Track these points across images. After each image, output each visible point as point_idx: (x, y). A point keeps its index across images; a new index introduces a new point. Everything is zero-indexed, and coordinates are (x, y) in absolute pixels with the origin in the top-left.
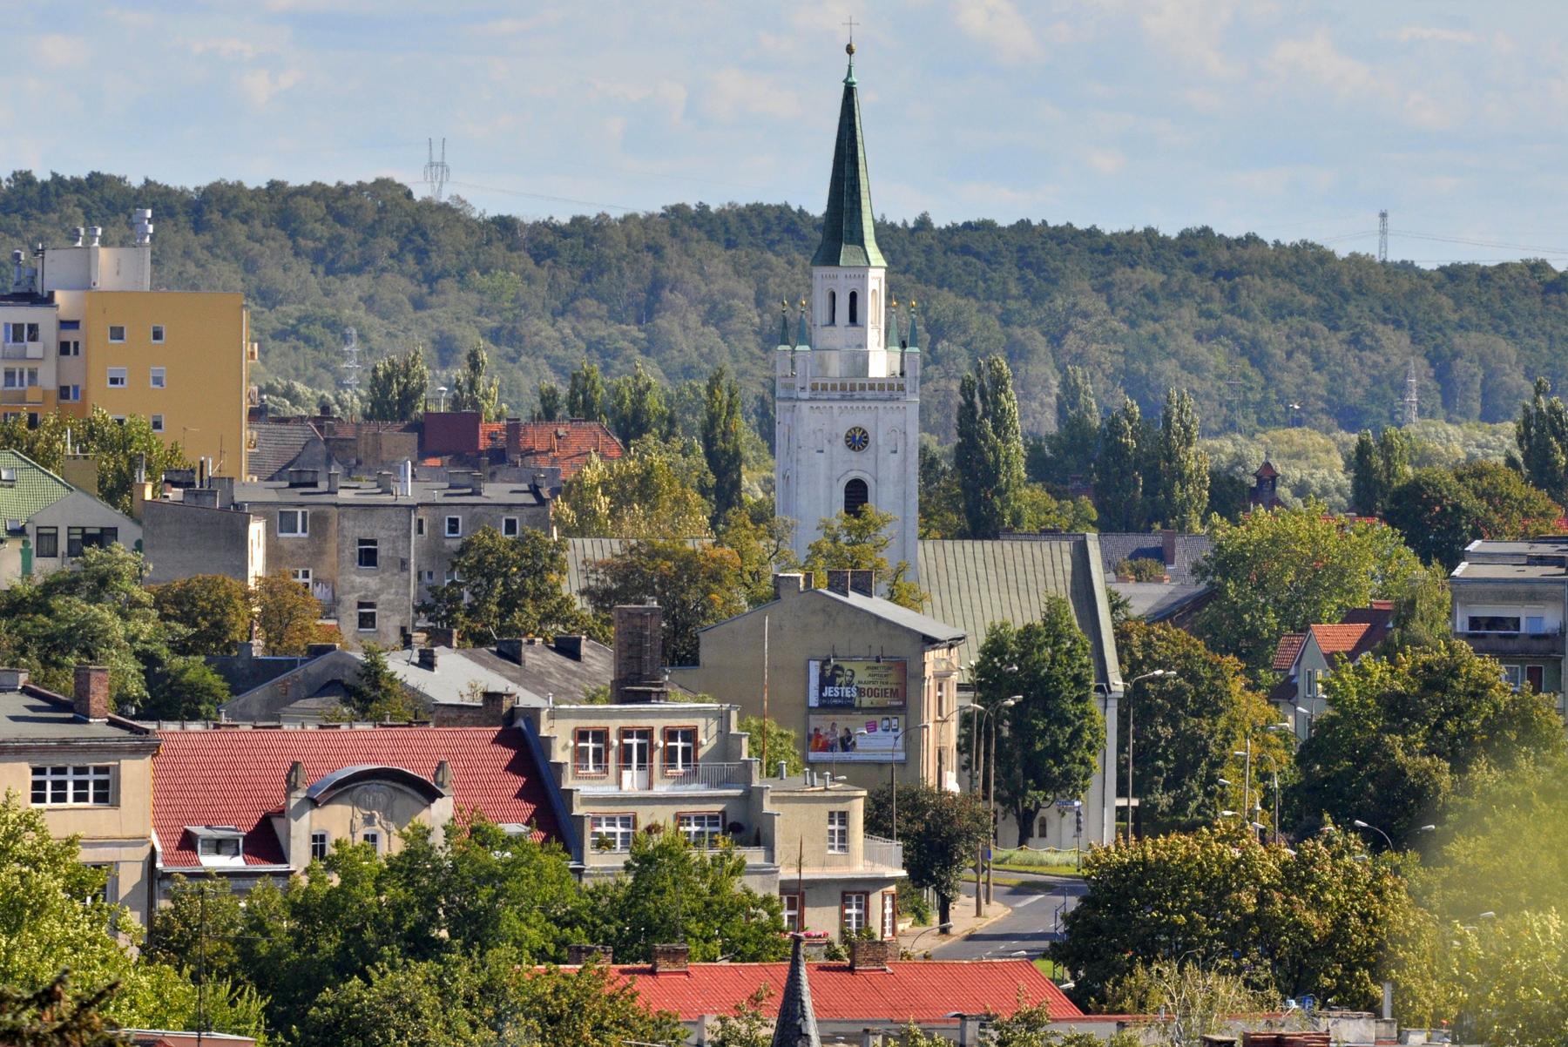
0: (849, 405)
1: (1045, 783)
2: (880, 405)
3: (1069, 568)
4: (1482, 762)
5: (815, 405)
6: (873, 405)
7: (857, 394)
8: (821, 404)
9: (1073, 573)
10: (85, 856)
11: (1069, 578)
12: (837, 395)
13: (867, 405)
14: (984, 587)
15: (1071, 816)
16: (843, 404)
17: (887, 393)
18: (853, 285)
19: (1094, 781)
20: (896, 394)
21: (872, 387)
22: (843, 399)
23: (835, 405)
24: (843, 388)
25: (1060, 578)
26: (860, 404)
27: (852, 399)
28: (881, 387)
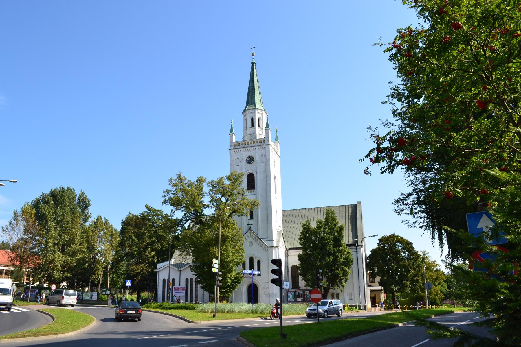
0: (246, 149)
1: (421, 11)
2: (257, 148)
3: (350, 212)
4: (493, 251)
5: (235, 150)
6: (254, 148)
7: (249, 145)
8: (237, 150)
9: (352, 213)
10: (114, 306)
11: (350, 214)
12: (242, 146)
13: (252, 148)
14: (344, 218)
15: (387, 99)
16: (244, 149)
17: (259, 144)
18: (251, 115)
19: (352, 271)
20: (262, 144)
21: (257, 142)
22: (245, 147)
23: (242, 150)
24: (245, 144)
25: (347, 214)
26: (250, 148)
27: (248, 147)
28: (261, 142)
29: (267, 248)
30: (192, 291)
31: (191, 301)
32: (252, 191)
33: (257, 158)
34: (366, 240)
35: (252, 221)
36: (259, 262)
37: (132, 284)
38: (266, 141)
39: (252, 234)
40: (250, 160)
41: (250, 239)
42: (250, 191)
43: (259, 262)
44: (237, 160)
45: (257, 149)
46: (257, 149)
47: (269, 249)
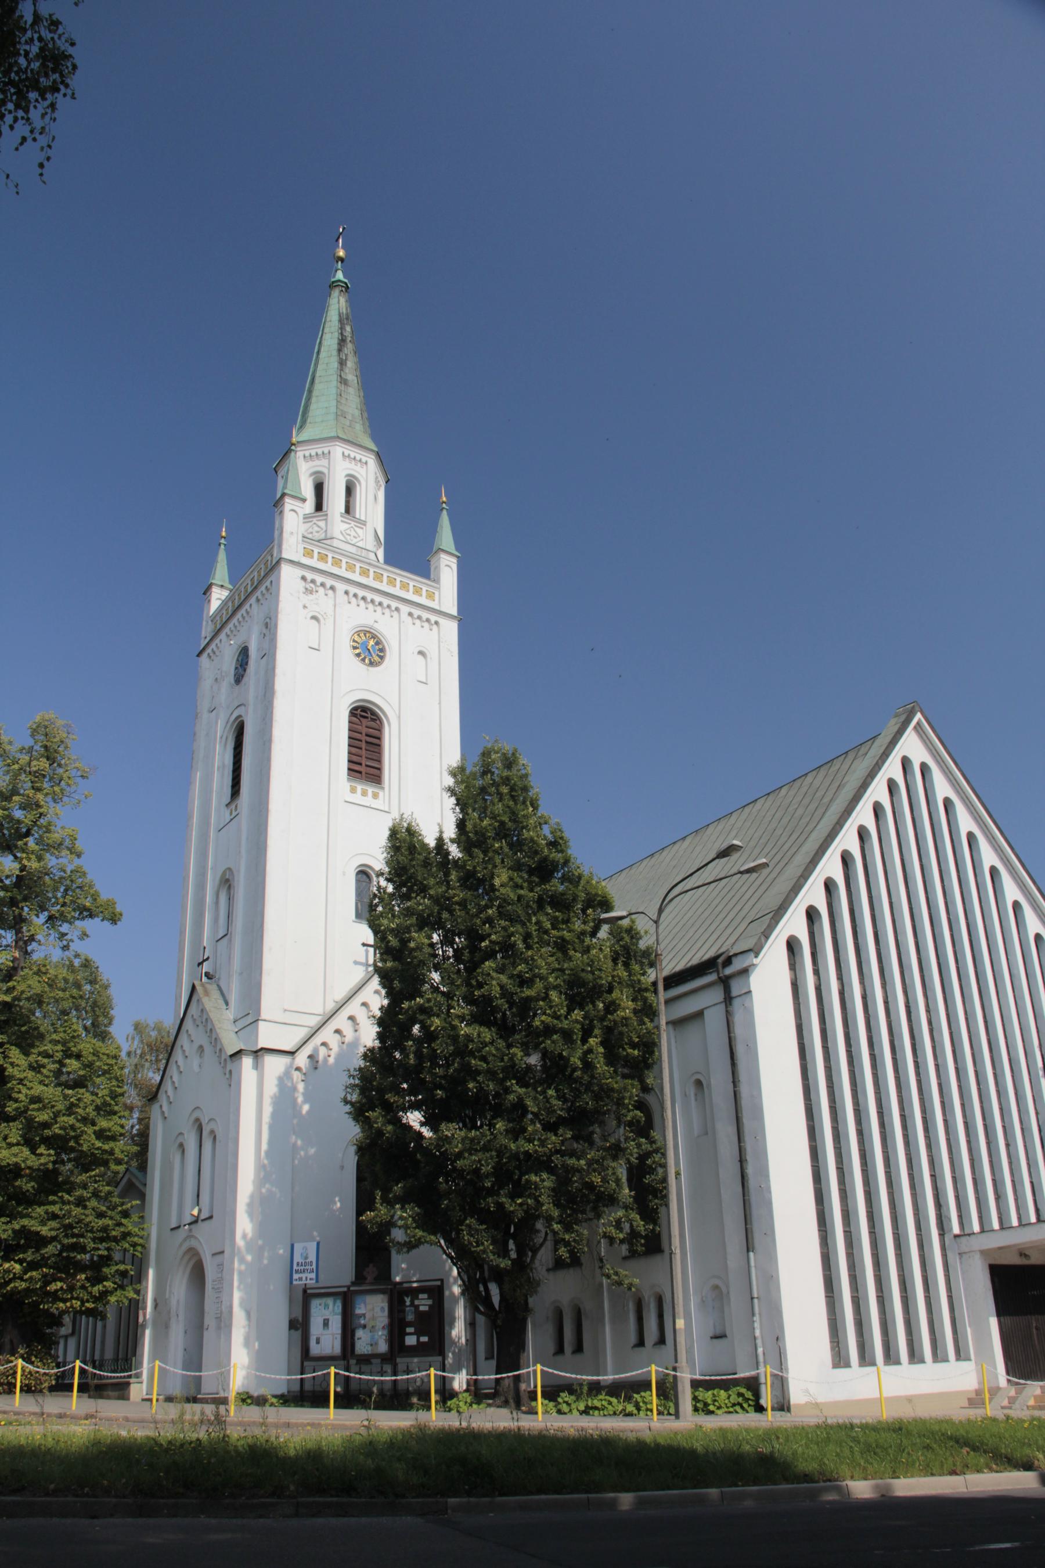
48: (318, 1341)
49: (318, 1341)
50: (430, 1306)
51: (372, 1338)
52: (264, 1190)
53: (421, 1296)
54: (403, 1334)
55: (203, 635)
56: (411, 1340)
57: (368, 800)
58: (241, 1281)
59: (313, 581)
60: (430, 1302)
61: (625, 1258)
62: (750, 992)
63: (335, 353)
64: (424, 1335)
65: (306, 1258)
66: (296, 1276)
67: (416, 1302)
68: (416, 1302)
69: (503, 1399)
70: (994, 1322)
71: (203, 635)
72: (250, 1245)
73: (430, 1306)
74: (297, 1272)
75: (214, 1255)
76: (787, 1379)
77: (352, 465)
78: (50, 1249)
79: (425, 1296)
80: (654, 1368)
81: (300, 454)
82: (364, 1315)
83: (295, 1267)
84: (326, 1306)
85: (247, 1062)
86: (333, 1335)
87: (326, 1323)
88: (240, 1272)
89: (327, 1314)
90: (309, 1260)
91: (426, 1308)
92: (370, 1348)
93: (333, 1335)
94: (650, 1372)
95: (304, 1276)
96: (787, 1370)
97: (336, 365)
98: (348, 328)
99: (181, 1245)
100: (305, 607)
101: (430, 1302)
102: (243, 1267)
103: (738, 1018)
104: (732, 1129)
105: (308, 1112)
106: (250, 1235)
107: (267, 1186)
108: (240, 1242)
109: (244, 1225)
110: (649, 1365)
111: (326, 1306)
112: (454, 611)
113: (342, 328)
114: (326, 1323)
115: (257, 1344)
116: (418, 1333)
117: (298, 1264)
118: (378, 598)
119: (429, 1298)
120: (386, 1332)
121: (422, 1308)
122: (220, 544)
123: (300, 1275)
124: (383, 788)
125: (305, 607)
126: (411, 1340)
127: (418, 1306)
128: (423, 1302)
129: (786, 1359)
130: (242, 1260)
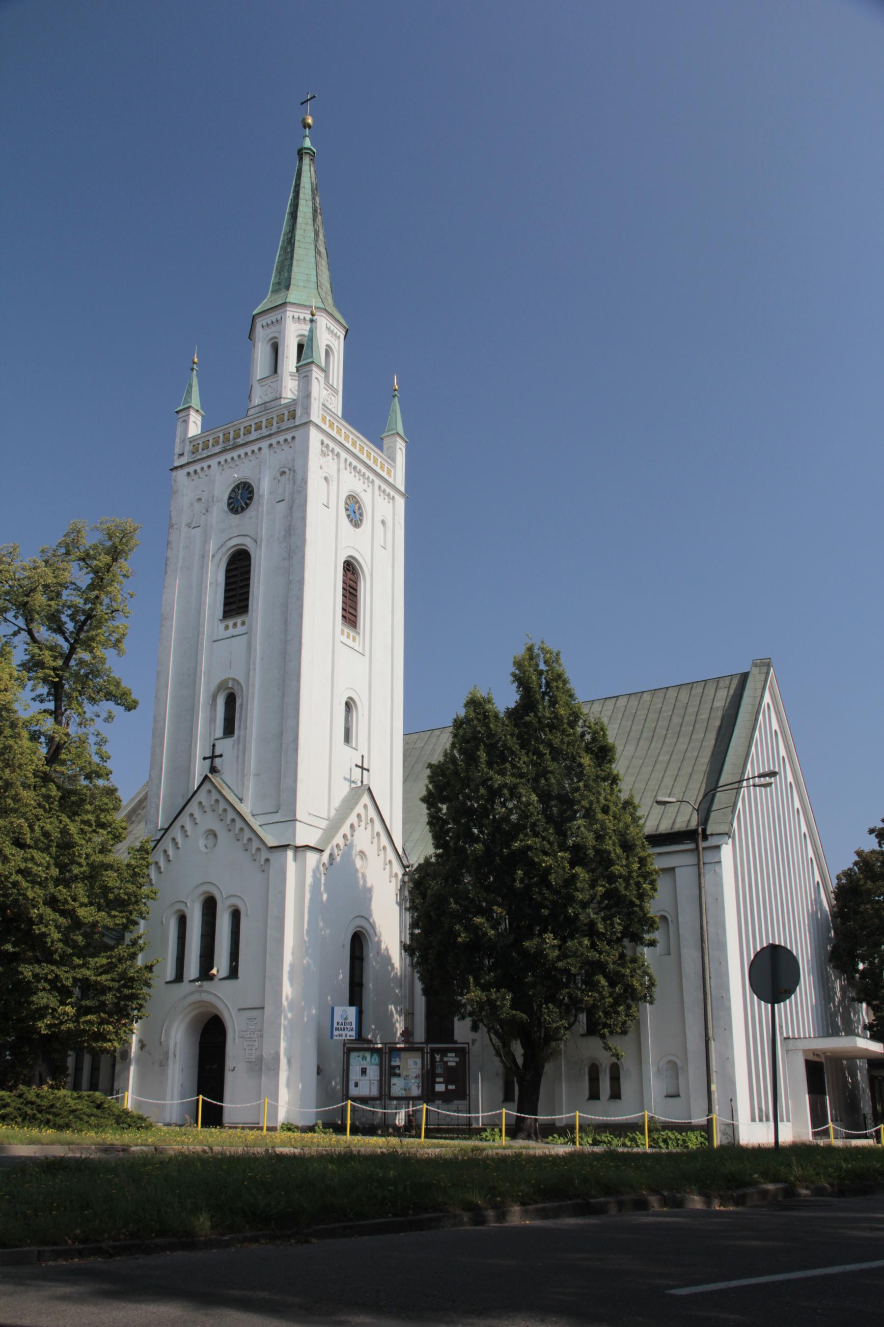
2: (264, 444)
9: (733, 696)
18: (271, 332)
27: (236, 447)
29: (264, 855)
30: (781, 1027)
31: (94, 1087)
32: (239, 621)
33: (264, 488)
34: (451, 724)
35: (225, 746)
36: (236, 915)
37: (875, 1009)
38: (299, 413)
39: (215, 795)
40: (242, 498)
41: (208, 821)
42: (230, 623)
43: (236, 915)
44: (197, 506)
45: (265, 449)
46: (265, 449)
47: (274, 857)
48: (356, 1085)
49: (356, 1085)
50: (457, 1062)
51: (406, 1084)
52: (305, 962)
53: (449, 1055)
54: (434, 1083)
55: (177, 450)
56: (440, 1088)
57: (349, 642)
58: (285, 1035)
59: (327, 446)
60: (457, 1059)
61: (582, 1035)
62: (720, 862)
63: (310, 222)
64: (452, 1084)
65: (346, 1019)
66: (336, 1033)
67: (445, 1059)
68: (445, 1059)
69: (526, 1133)
70: (807, 1096)
71: (177, 450)
72: (291, 1004)
73: (457, 1062)
74: (337, 1029)
75: (239, 1010)
76: (738, 1126)
77: (333, 339)
78: (109, 998)
79: (453, 1055)
80: (578, 1113)
81: (289, 314)
82: (399, 1067)
83: (335, 1025)
84: (364, 1058)
85: (290, 854)
86: (370, 1080)
87: (364, 1071)
88: (285, 1027)
89: (364, 1064)
90: (349, 1021)
91: (454, 1064)
92: (404, 1092)
93: (370, 1080)
94: (575, 1116)
95: (344, 1033)
96: (737, 1121)
97: (313, 235)
98: (318, 199)
99: (185, 997)
100: (321, 467)
101: (457, 1059)
102: (286, 1023)
103: (708, 879)
104: (697, 954)
105: (327, 900)
106: (290, 997)
107: (307, 958)
108: (285, 1003)
109: (287, 989)
110: (575, 1111)
111: (364, 1058)
112: (403, 489)
113: (314, 199)
114: (364, 1071)
115: (300, 1086)
116: (447, 1082)
117: (338, 1023)
118: (363, 470)
119: (456, 1056)
120: (419, 1080)
121: (450, 1064)
122: (192, 369)
123: (340, 1032)
124: (359, 633)
125: (321, 467)
126: (440, 1088)
127: (447, 1062)
128: (451, 1059)
129: (737, 1114)
130: (286, 1017)
